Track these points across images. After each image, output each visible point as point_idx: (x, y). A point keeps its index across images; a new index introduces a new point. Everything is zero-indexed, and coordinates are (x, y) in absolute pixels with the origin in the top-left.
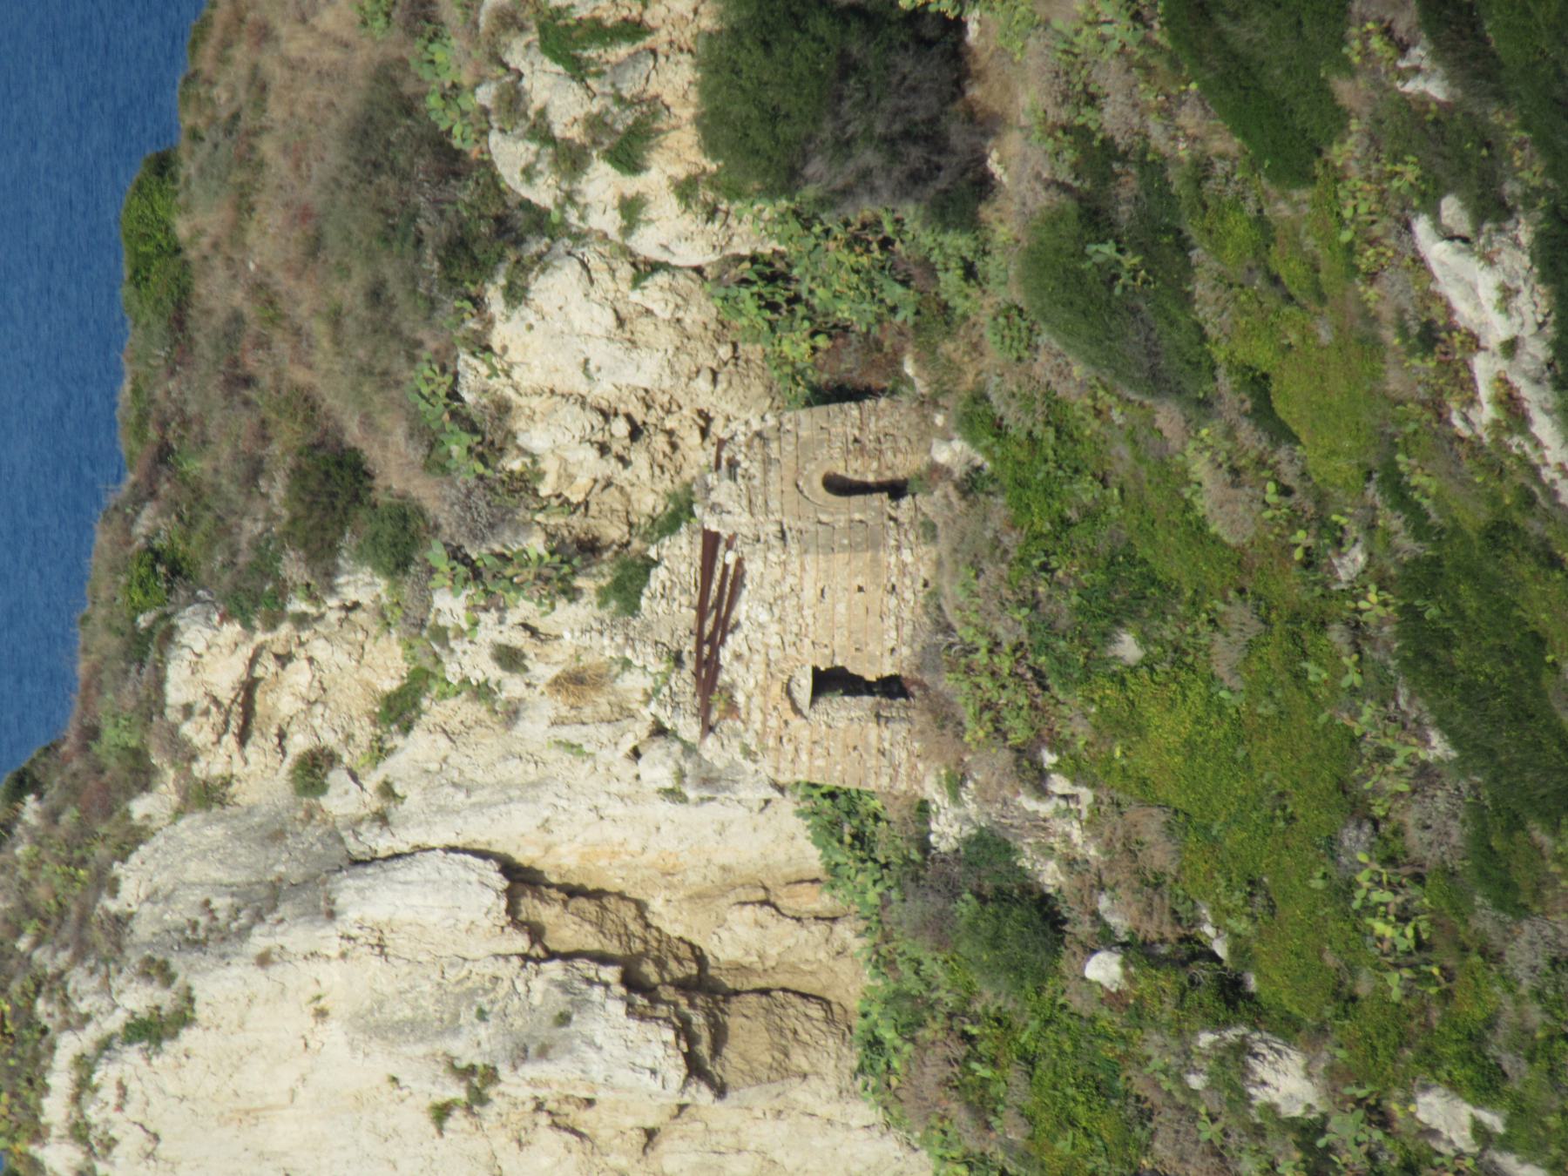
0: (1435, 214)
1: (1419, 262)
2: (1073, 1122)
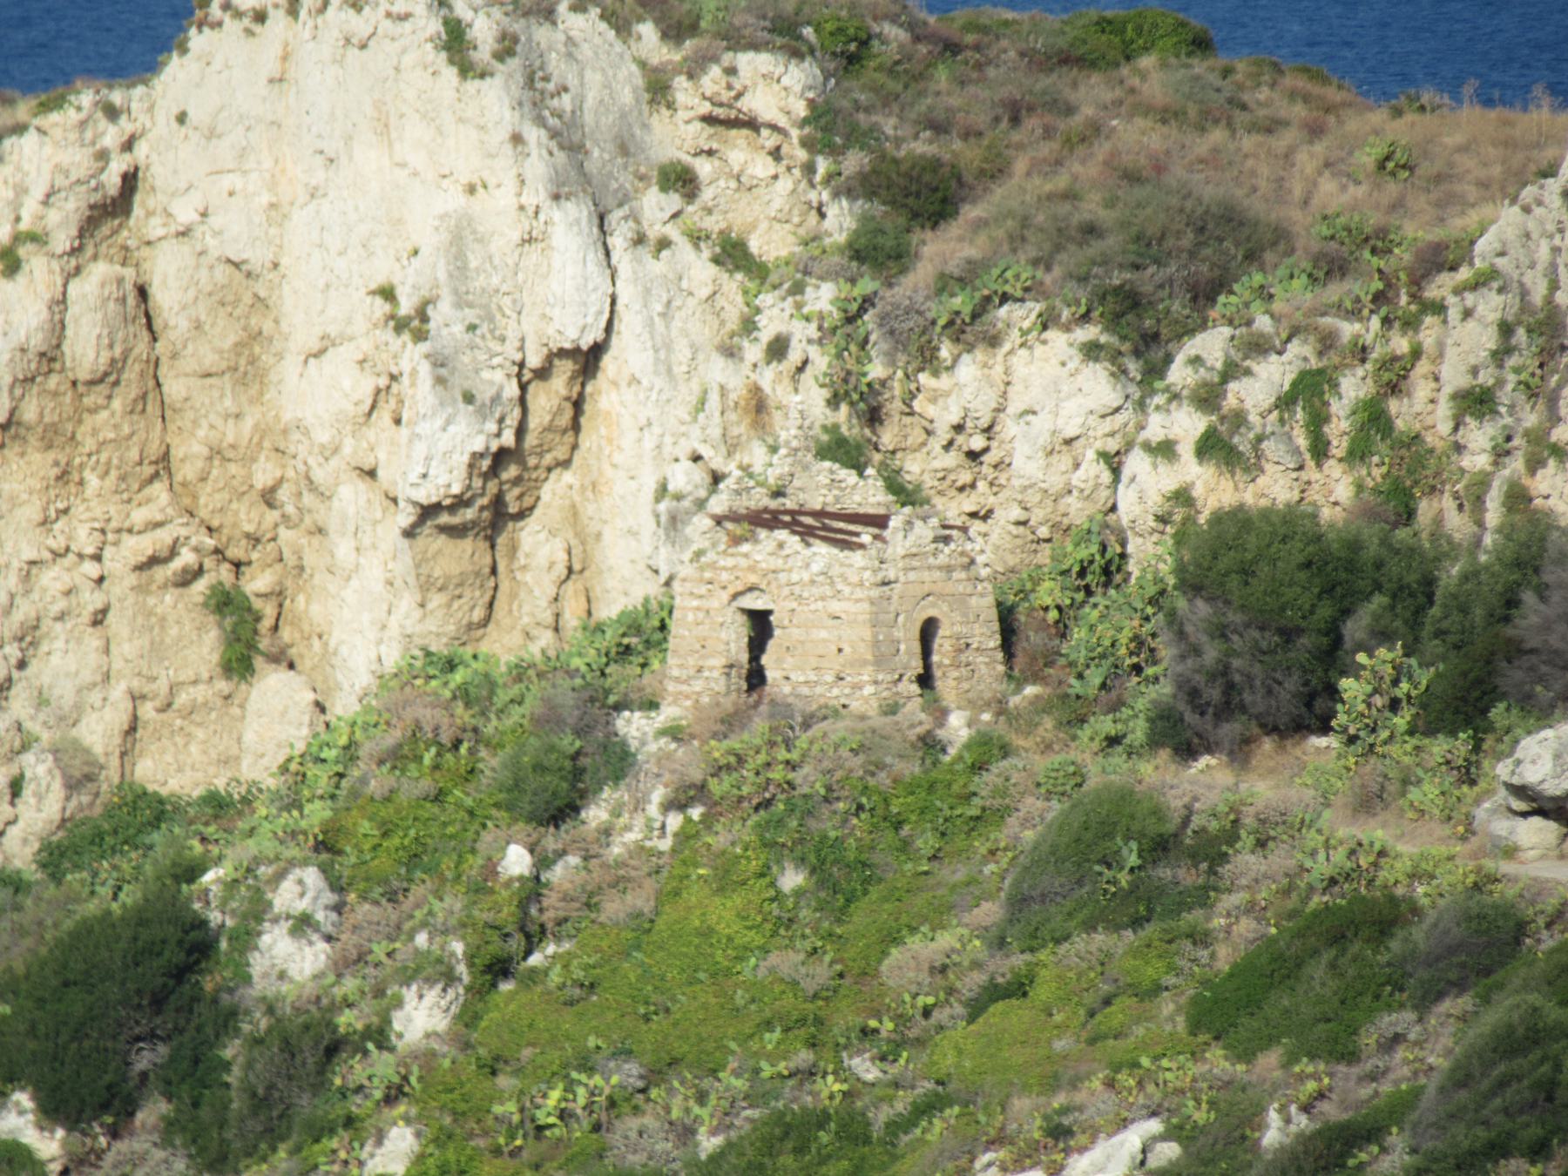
0: (1163, 1138)
1: (1124, 1124)
2: (385, 835)
